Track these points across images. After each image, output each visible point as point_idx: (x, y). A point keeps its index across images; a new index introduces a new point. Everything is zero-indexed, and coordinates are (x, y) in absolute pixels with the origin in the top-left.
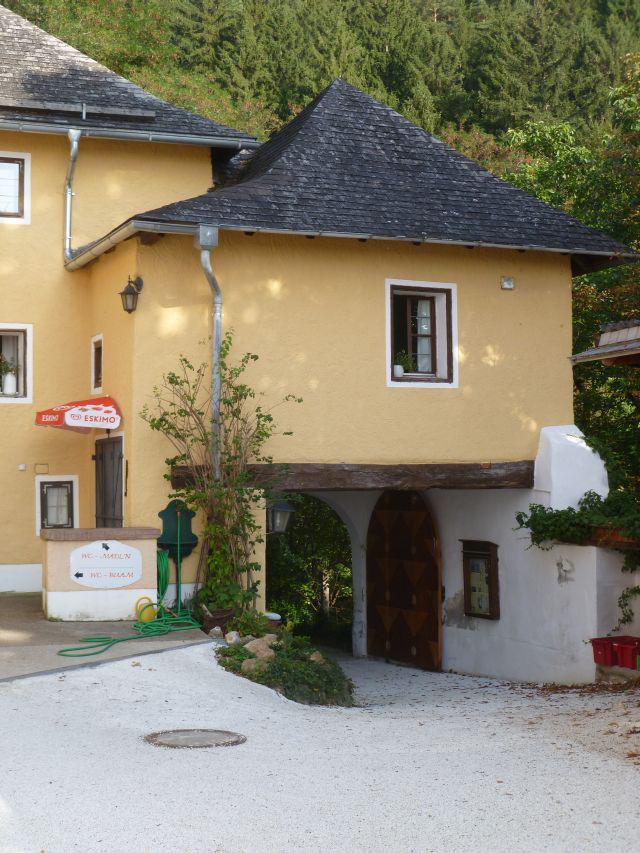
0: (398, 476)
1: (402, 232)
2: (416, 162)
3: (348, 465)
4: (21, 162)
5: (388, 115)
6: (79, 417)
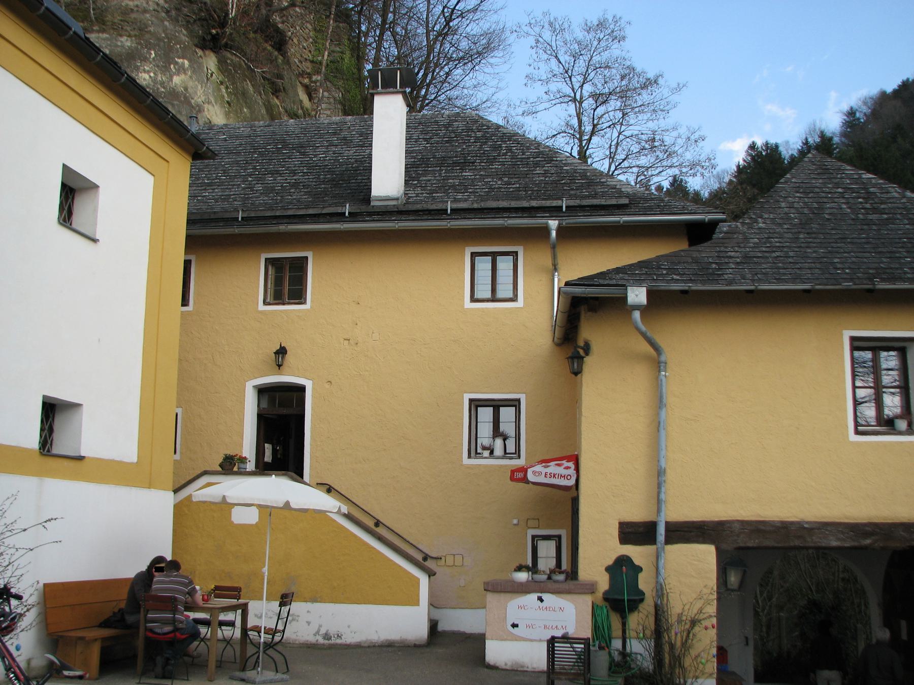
0: (867, 535)
1: (851, 280)
2: (885, 216)
3: (807, 523)
4: (515, 254)
5: (860, 178)
6: (540, 473)
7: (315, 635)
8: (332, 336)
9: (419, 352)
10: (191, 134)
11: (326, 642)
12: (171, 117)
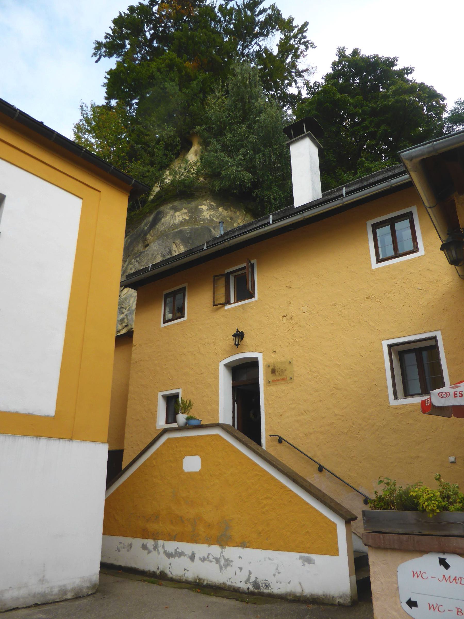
4: (409, 216)
7: (246, 582)
8: (273, 316)
9: (340, 314)
10: (19, 113)
11: (256, 591)
12: (85, 151)
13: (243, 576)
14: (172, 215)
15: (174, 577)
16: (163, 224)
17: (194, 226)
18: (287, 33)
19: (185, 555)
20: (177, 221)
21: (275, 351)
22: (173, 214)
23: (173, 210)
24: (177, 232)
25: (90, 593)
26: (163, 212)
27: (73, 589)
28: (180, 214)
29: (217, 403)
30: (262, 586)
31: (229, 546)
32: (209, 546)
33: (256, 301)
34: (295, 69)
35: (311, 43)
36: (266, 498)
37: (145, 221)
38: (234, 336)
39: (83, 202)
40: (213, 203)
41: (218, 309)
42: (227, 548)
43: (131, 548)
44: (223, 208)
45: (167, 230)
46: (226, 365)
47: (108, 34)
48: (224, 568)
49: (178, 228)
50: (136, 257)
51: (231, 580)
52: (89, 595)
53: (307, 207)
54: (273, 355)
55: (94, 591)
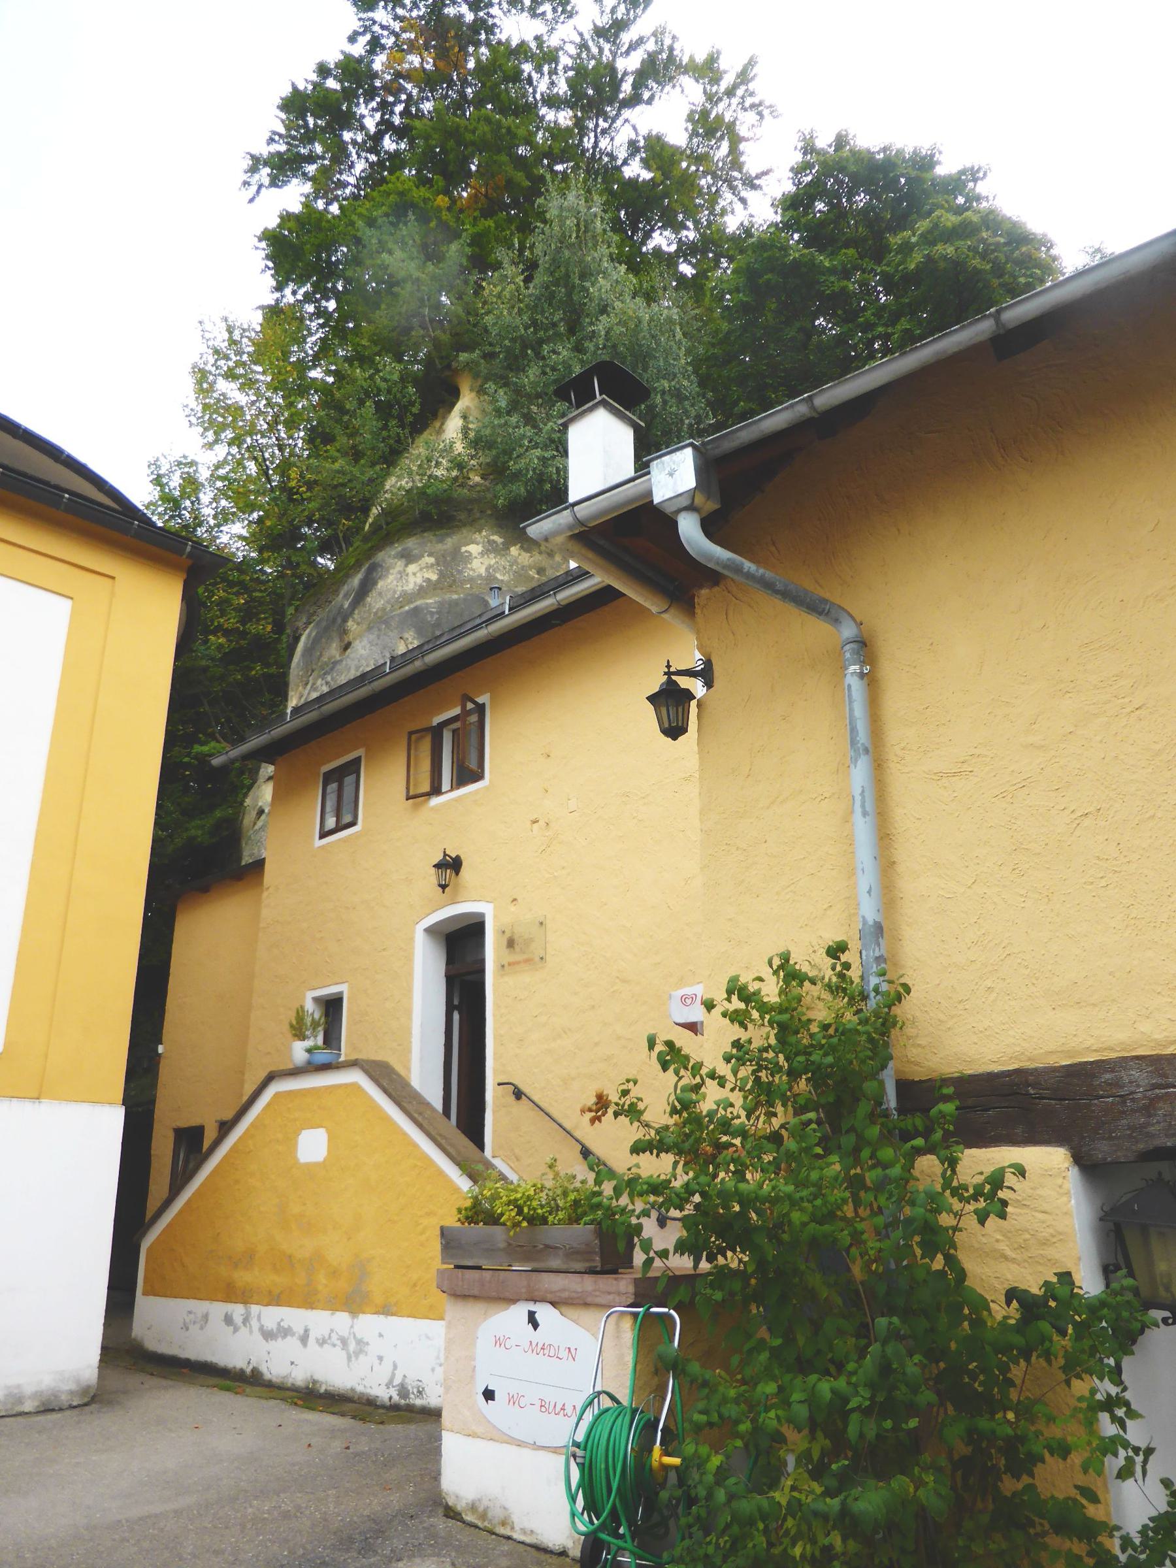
11: (403, 1402)
13: (383, 1374)
14: (400, 572)
15: (274, 1380)
16: (380, 594)
17: (447, 596)
18: (708, 87)
19: (293, 1334)
20: (411, 586)
21: (515, 900)
22: (401, 569)
23: (403, 560)
24: (407, 612)
25: (75, 1403)
26: (381, 566)
27: (36, 1395)
28: (418, 568)
29: (409, 1012)
30: (413, 1393)
31: (364, 1313)
32: (332, 1314)
33: (487, 788)
34: (741, 172)
35: (771, 106)
36: (428, 1214)
37: (346, 588)
38: (438, 866)
39: (73, 607)
40: (495, 538)
41: (416, 807)
42: (361, 1316)
43: (206, 1322)
44: (522, 548)
45: (389, 607)
46: (431, 931)
47: (274, 133)
48: (353, 1359)
49: (412, 602)
50: (325, 674)
51: (364, 1382)
52: (72, 1407)
53: (575, 575)
54: (513, 908)
55: (86, 1400)
